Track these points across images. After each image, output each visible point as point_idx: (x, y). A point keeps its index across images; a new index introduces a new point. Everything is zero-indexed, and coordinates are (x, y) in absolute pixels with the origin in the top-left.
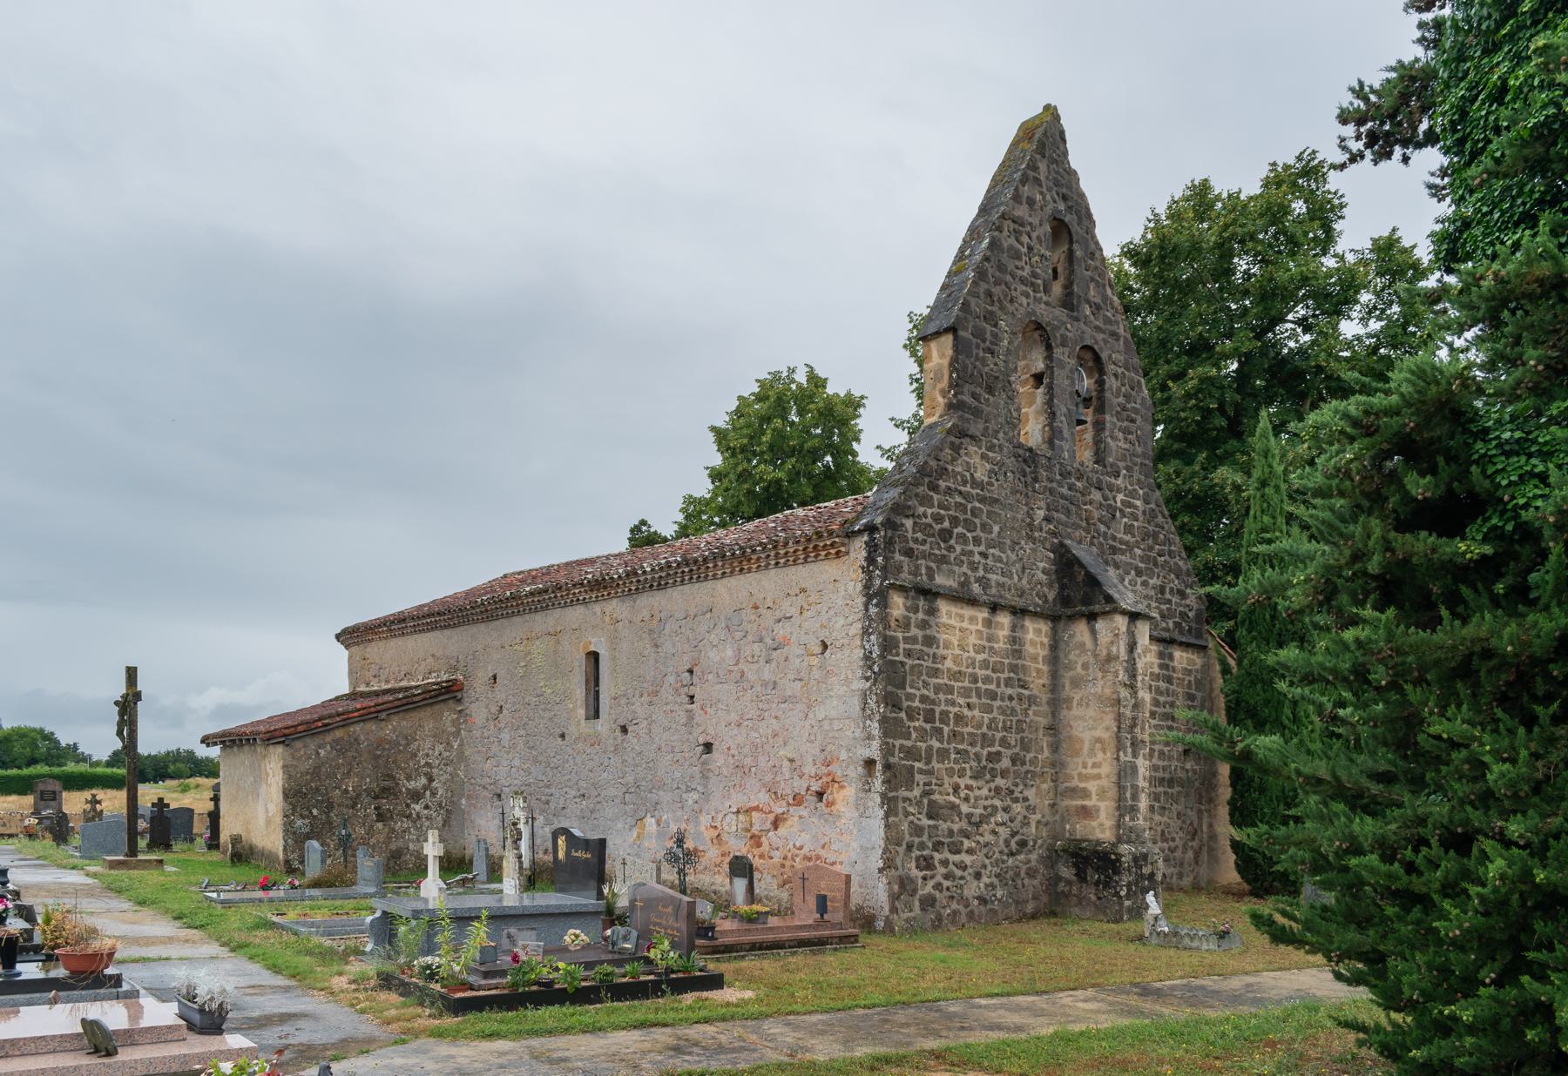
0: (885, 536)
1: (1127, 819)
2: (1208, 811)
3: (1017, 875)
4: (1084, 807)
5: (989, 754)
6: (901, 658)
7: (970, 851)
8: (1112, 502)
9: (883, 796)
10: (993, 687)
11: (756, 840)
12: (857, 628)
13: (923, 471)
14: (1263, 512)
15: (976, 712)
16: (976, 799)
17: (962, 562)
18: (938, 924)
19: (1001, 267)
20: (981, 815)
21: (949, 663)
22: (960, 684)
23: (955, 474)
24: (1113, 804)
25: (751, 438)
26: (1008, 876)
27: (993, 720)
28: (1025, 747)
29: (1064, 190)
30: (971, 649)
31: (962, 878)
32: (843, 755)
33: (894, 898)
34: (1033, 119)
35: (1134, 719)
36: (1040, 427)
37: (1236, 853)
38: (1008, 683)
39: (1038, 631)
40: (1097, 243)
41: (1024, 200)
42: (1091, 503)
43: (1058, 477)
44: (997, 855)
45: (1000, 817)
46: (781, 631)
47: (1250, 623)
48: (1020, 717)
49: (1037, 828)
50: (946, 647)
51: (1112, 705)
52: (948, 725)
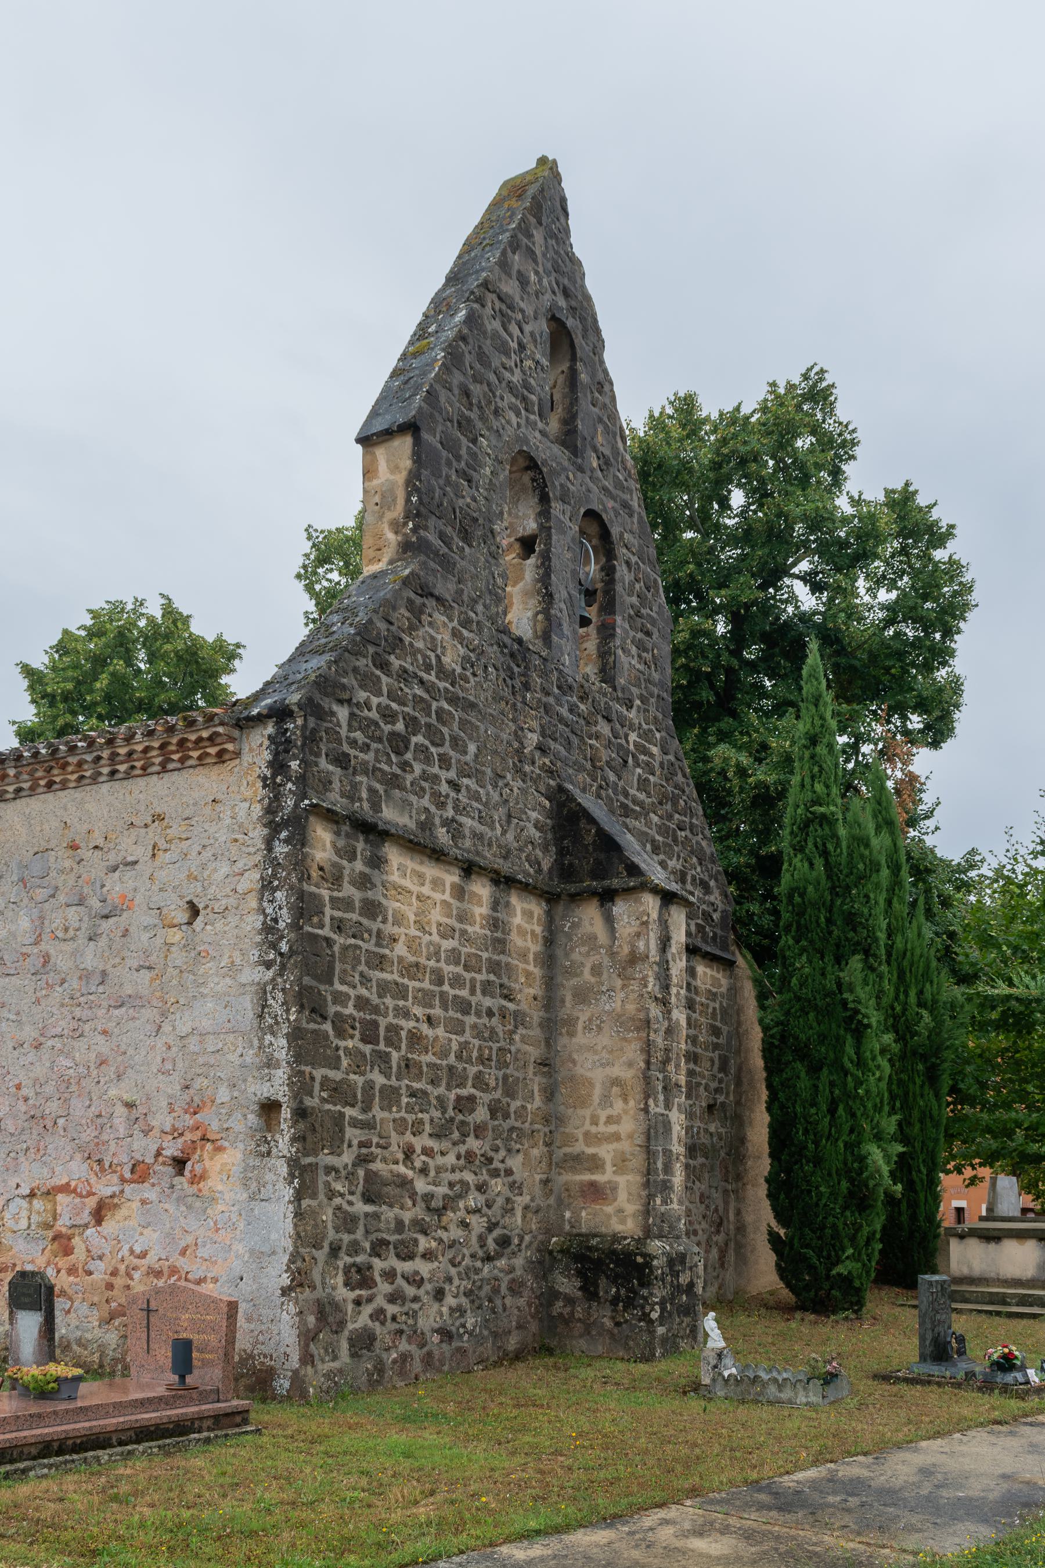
0: (304, 727)
1: (658, 1201)
2: (735, 1191)
3: (496, 1290)
4: (593, 1184)
5: (459, 1098)
6: (326, 932)
7: (428, 1256)
8: (623, 742)
9: (293, 1163)
10: (464, 993)
11: (63, 1243)
12: (252, 880)
13: (365, 635)
14: (813, 778)
15: (440, 1031)
16: (439, 1170)
17: (423, 789)
18: (377, 1379)
19: (482, 358)
20: (445, 1197)
21: (401, 949)
22: (417, 984)
23: (415, 651)
24: (637, 1179)
25: (79, 683)
26: (482, 1294)
27: (464, 1046)
28: (510, 1090)
29: (566, 281)
30: (434, 930)
31: (416, 1299)
32: (223, 1094)
33: (308, 1337)
34: (523, 176)
35: (667, 1050)
36: (530, 614)
37: (775, 1250)
38: (487, 988)
39: (528, 914)
40: (606, 372)
41: (514, 273)
42: (597, 738)
43: (556, 691)
44: (467, 1261)
45: (473, 1200)
46: (117, 886)
47: (799, 927)
48: (502, 1044)
49: (524, 1217)
50: (397, 922)
51: (638, 1029)
52: (398, 1048)
